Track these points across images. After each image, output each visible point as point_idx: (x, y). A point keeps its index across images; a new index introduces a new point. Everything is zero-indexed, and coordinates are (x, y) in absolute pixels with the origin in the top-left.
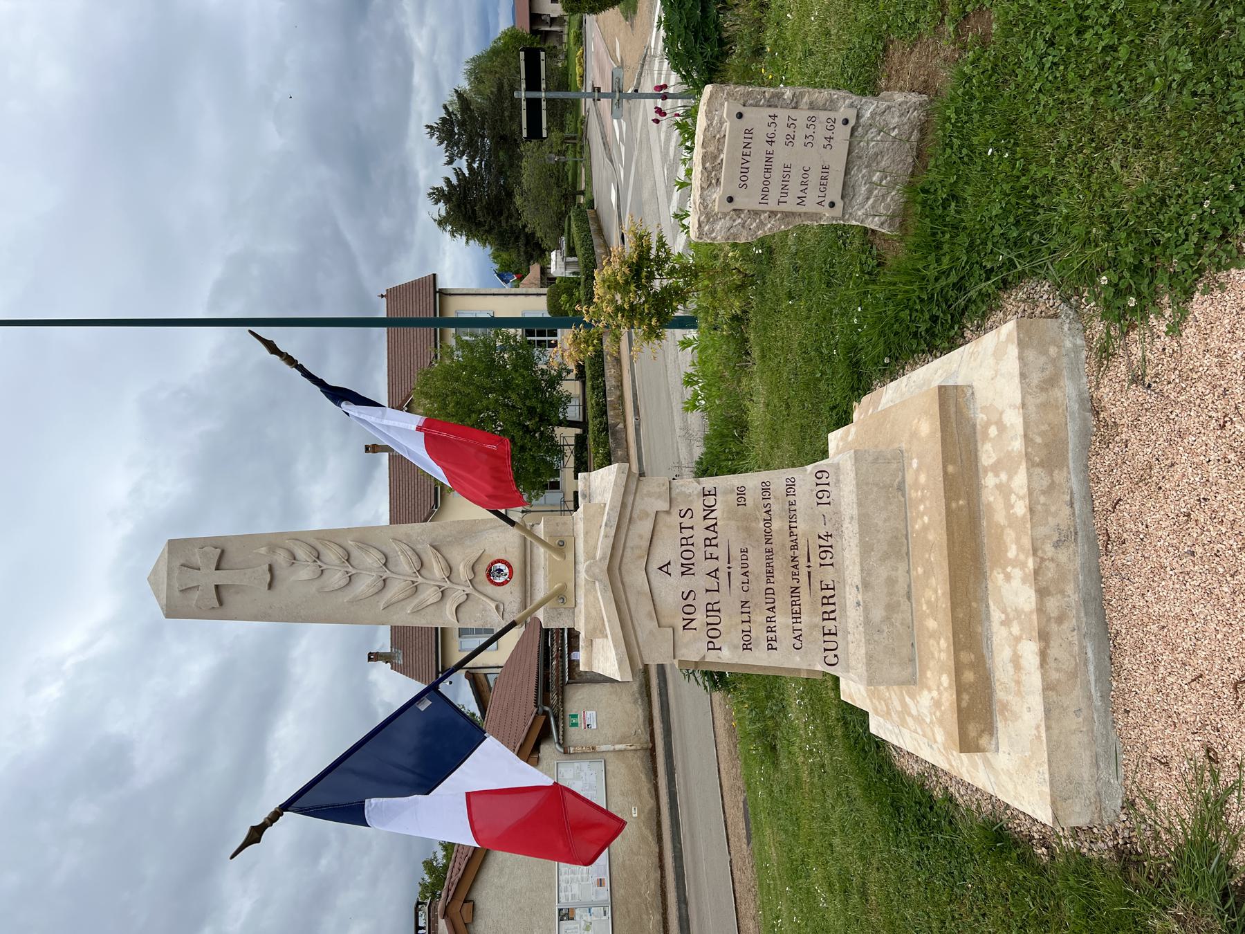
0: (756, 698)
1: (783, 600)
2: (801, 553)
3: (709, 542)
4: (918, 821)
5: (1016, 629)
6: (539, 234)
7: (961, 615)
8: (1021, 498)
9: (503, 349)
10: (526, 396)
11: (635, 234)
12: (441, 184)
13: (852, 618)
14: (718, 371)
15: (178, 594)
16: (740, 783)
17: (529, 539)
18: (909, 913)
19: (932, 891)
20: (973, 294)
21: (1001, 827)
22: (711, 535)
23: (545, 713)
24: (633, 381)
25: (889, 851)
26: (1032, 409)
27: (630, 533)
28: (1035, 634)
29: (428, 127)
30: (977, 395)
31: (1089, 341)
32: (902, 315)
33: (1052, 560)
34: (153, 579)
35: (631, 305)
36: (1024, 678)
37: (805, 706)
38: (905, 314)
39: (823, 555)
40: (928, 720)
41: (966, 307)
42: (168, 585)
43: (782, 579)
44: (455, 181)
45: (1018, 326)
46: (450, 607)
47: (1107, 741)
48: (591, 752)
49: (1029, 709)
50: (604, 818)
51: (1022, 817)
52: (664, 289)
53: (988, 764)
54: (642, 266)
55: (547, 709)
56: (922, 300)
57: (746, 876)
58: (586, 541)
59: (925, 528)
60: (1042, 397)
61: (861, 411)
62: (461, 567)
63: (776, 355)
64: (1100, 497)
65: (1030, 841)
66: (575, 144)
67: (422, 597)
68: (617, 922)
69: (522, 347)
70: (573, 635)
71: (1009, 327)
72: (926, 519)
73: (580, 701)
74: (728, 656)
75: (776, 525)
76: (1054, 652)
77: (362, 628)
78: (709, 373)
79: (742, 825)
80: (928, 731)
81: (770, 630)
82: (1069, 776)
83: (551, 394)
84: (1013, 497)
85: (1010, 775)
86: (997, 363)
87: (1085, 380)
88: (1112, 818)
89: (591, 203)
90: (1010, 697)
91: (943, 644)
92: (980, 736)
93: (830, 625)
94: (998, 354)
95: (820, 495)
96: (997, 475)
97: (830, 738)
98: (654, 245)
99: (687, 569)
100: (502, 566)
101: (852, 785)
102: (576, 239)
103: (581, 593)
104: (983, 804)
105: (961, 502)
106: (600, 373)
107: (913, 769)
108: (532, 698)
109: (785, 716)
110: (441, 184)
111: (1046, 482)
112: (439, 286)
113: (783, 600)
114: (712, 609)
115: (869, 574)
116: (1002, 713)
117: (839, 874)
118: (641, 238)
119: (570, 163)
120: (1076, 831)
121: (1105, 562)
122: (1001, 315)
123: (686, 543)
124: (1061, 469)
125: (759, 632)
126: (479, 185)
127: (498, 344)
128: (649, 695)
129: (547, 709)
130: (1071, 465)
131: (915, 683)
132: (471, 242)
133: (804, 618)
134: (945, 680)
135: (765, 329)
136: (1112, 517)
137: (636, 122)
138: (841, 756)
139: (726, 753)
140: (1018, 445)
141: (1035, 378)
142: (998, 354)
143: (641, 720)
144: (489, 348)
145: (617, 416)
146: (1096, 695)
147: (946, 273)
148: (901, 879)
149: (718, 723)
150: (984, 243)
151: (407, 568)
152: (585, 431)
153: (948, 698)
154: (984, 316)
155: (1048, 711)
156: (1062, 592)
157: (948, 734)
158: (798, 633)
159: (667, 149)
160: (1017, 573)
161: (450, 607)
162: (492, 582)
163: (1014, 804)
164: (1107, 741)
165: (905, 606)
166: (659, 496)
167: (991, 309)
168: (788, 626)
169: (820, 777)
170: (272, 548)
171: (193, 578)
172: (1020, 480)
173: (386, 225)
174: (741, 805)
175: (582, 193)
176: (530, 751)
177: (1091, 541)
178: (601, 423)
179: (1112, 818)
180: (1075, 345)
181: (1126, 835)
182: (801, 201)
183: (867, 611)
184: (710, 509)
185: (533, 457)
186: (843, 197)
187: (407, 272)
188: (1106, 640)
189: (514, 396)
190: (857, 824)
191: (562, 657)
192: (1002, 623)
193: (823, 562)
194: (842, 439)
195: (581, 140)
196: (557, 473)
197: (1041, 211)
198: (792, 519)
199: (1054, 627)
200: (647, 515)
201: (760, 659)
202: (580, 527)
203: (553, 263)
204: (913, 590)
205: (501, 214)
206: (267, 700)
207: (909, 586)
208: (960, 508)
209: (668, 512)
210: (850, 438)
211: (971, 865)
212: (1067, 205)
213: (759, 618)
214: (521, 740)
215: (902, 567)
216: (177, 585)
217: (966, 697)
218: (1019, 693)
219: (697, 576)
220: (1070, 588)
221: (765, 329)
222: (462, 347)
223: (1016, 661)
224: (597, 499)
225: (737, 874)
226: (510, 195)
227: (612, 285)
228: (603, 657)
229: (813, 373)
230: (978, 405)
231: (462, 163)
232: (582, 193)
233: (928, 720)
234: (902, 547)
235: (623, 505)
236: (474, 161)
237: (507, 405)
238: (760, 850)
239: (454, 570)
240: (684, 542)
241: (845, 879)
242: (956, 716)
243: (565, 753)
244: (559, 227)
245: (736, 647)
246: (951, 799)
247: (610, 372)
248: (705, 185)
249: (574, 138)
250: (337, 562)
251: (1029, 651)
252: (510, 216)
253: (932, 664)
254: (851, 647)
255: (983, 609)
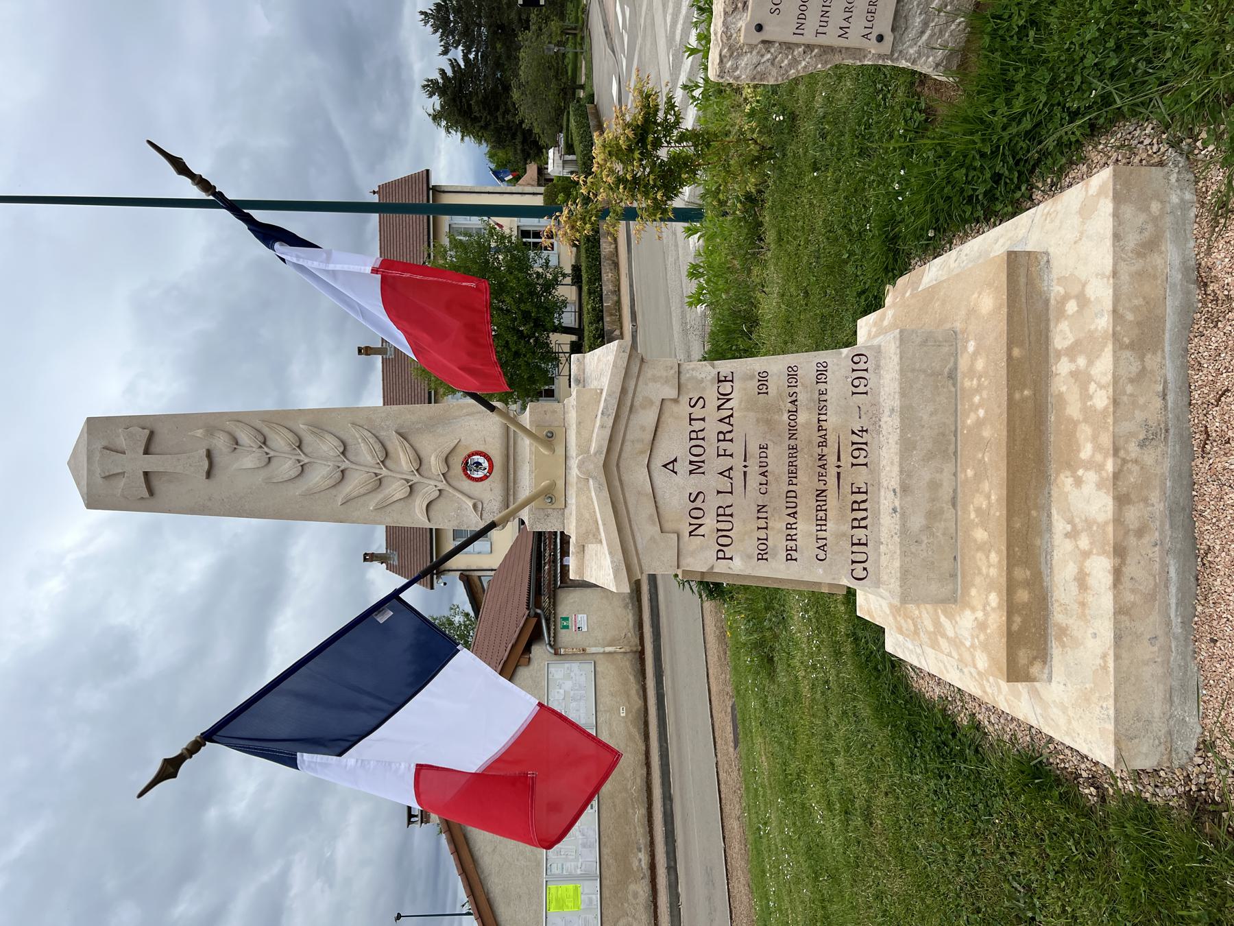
0: (756, 613)
1: (806, 504)
2: (830, 452)
3: (723, 437)
4: (938, 747)
5: (1084, 542)
6: (536, 130)
7: (1018, 525)
8: (1102, 387)
9: (498, 250)
10: (521, 300)
11: (641, 92)
12: (436, 76)
13: (886, 523)
14: (727, 262)
15: (100, 481)
16: (729, 689)
17: (512, 428)
18: (921, 843)
19: (950, 821)
20: (1050, 143)
21: (1041, 762)
22: (726, 428)
23: (537, 615)
24: (631, 286)
25: (901, 776)
26: (1125, 277)
27: (631, 423)
28: (1110, 548)
29: (422, 13)
30: (1054, 263)
31: (1201, 195)
32: (956, 174)
33: (1136, 462)
34: (73, 464)
35: (634, 177)
36: (1090, 599)
37: (810, 620)
38: (960, 174)
39: (856, 453)
40: (968, 644)
41: (1039, 161)
42: (89, 470)
43: (806, 481)
44: (450, 73)
45: (1116, 175)
46: (419, 503)
47: (1185, 673)
48: (582, 654)
49: (1095, 635)
50: (591, 748)
51: (1067, 752)
52: (674, 158)
53: (1035, 694)
54: (648, 128)
55: (539, 611)
56: (983, 155)
57: (732, 778)
58: (578, 433)
59: (980, 423)
60: (1139, 265)
61: (892, 296)
62: (433, 458)
63: (795, 238)
64: (1201, 387)
65: (1075, 779)
66: (575, 35)
67: (387, 492)
68: (604, 815)
69: (516, 248)
70: (565, 540)
71: (1103, 177)
72: (981, 413)
73: (569, 603)
74: (740, 566)
75: (802, 417)
76: (1131, 569)
77: (360, 528)
78: (716, 263)
79: (729, 729)
80: (967, 657)
81: (790, 538)
82: (1137, 712)
83: (546, 298)
84: (1093, 387)
85: (1064, 709)
86: (1083, 223)
87: (1192, 244)
88: (1184, 760)
89: (591, 98)
90: (1071, 621)
91: (994, 557)
92: (1031, 663)
93: (860, 534)
94: (1086, 211)
95: (856, 383)
96: (1072, 360)
97: (837, 654)
98: (662, 106)
99: (696, 467)
100: (481, 459)
101: (860, 705)
102: (575, 135)
103: (572, 492)
104: (1019, 735)
105: (1026, 393)
106: (597, 277)
107: (933, 692)
108: (525, 600)
109: (785, 627)
110: (436, 76)
111: (1135, 368)
112: (433, 183)
113: (806, 504)
114: (724, 514)
115: (909, 476)
116: (1059, 638)
117: (841, 794)
118: (648, 96)
119: (570, 55)
120: (1137, 775)
121: (1201, 465)
122: (1084, 168)
123: (696, 437)
124: (1154, 353)
125: (777, 541)
126: (475, 78)
127: (493, 245)
128: (639, 600)
129: (539, 611)
130: (1167, 348)
131: (956, 601)
132: (467, 139)
133: (830, 525)
134: (994, 599)
135: (783, 208)
136: (1215, 411)
137: (640, 6)
138: (849, 671)
139: (716, 659)
140: (1103, 323)
141: (1132, 240)
142: (1086, 211)
143: (631, 623)
144: (484, 249)
145: (613, 322)
146: (1176, 621)
147: (1018, 119)
148: (913, 806)
149: (708, 629)
150: (1070, 78)
151: (369, 458)
152: (581, 338)
153: (997, 620)
154: (1062, 172)
155: (1118, 638)
156: (1145, 500)
157: (992, 659)
158: (821, 543)
159: (673, 32)
160: (1091, 477)
161: (419, 503)
162: (469, 477)
163: (1057, 737)
164: (1185, 673)
165: (949, 513)
166: (667, 381)
167: (1071, 163)
168: (811, 535)
169: (823, 693)
170: (211, 430)
171: (116, 463)
172: (1103, 366)
173: (380, 120)
174: (729, 710)
175: (582, 87)
176: (510, 666)
177: (1185, 440)
178: (597, 329)
179: (1184, 760)
180: (1182, 200)
181: (1201, 780)
182: (844, 32)
183: (904, 518)
184: (726, 398)
185: (528, 364)
186: (893, 30)
187: (400, 168)
188: (1194, 558)
189: (508, 300)
190: (865, 745)
191: (555, 561)
192: (1067, 535)
193: (855, 461)
194: (875, 324)
195: (582, 30)
196: (551, 381)
197: (1150, 32)
198: (822, 409)
199: (1132, 541)
200: (652, 403)
201: (777, 570)
202: (572, 416)
203: (550, 161)
204: (960, 495)
205: (497, 109)
206: (267, 595)
207: (955, 491)
208: (1024, 400)
209: (676, 401)
210: (886, 323)
211: (999, 800)
212: (1189, 19)
213: (778, 525)
214: (513, 641)
215: (948, 468)
216: (98, 471)
217: (1018, 619)
218: (1083, 616)
219: (707, 476)
220: (1155, 496)
221: (783, 208)
222: (456, 247)
223: (1082, 580)
224: (594, 385)
225: (723, 775)
226: (507, 88)
227: (614, 151)
228: (597, 564)
229: (839, 254)
230: (1055, 274)
231: (458, 53)
232: (582, 87)
233: (968, 644)
234: (947, 445)
235: (624, 390)
236: (470, 52)
237: (502, 309)
238: (747, 755)
239: (425, 462)
240: (694, 435)
241: (847, 799)
242: (1004, 640)
243: (556, 654)
244: (557, 123)
245: (750, 557)
246: (977, 726)
247: (607, 276)
248: (729, 10)
249: (575, 29)
250: (287, 449)
251: (1100, 568)
252: (507, 111)
253: (978, 580)
254: (884, 560)
255: (1044, 518)
